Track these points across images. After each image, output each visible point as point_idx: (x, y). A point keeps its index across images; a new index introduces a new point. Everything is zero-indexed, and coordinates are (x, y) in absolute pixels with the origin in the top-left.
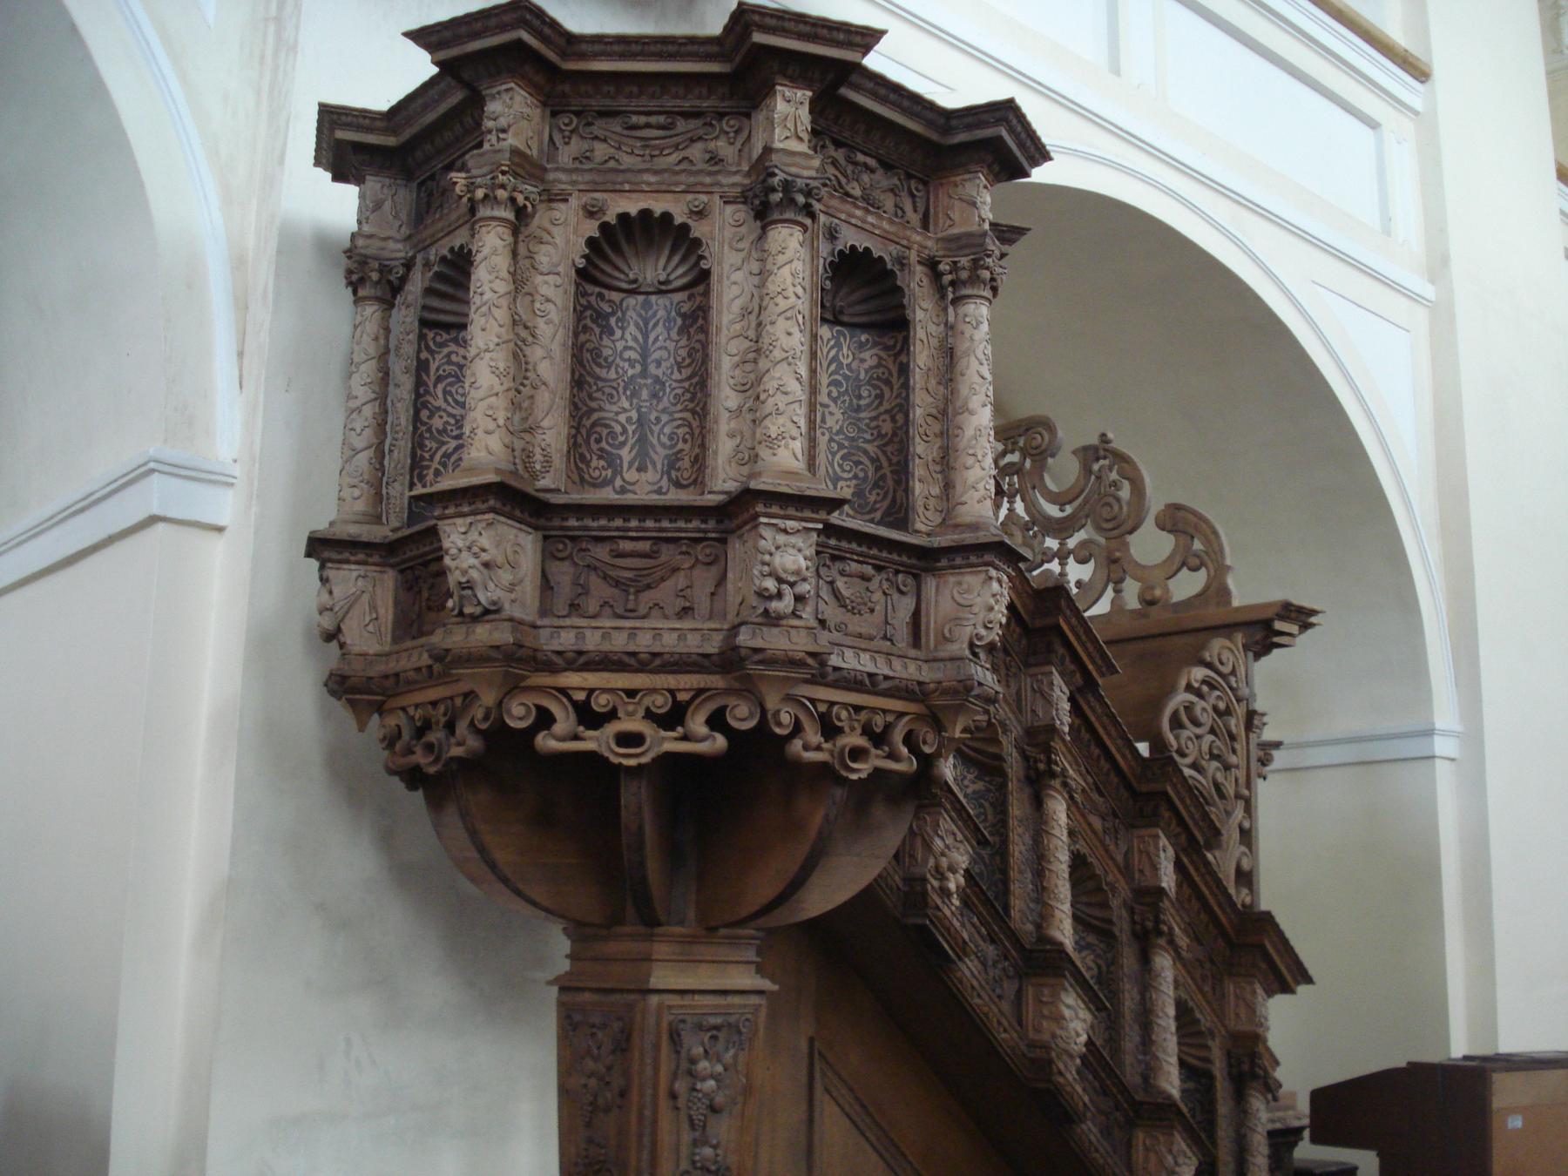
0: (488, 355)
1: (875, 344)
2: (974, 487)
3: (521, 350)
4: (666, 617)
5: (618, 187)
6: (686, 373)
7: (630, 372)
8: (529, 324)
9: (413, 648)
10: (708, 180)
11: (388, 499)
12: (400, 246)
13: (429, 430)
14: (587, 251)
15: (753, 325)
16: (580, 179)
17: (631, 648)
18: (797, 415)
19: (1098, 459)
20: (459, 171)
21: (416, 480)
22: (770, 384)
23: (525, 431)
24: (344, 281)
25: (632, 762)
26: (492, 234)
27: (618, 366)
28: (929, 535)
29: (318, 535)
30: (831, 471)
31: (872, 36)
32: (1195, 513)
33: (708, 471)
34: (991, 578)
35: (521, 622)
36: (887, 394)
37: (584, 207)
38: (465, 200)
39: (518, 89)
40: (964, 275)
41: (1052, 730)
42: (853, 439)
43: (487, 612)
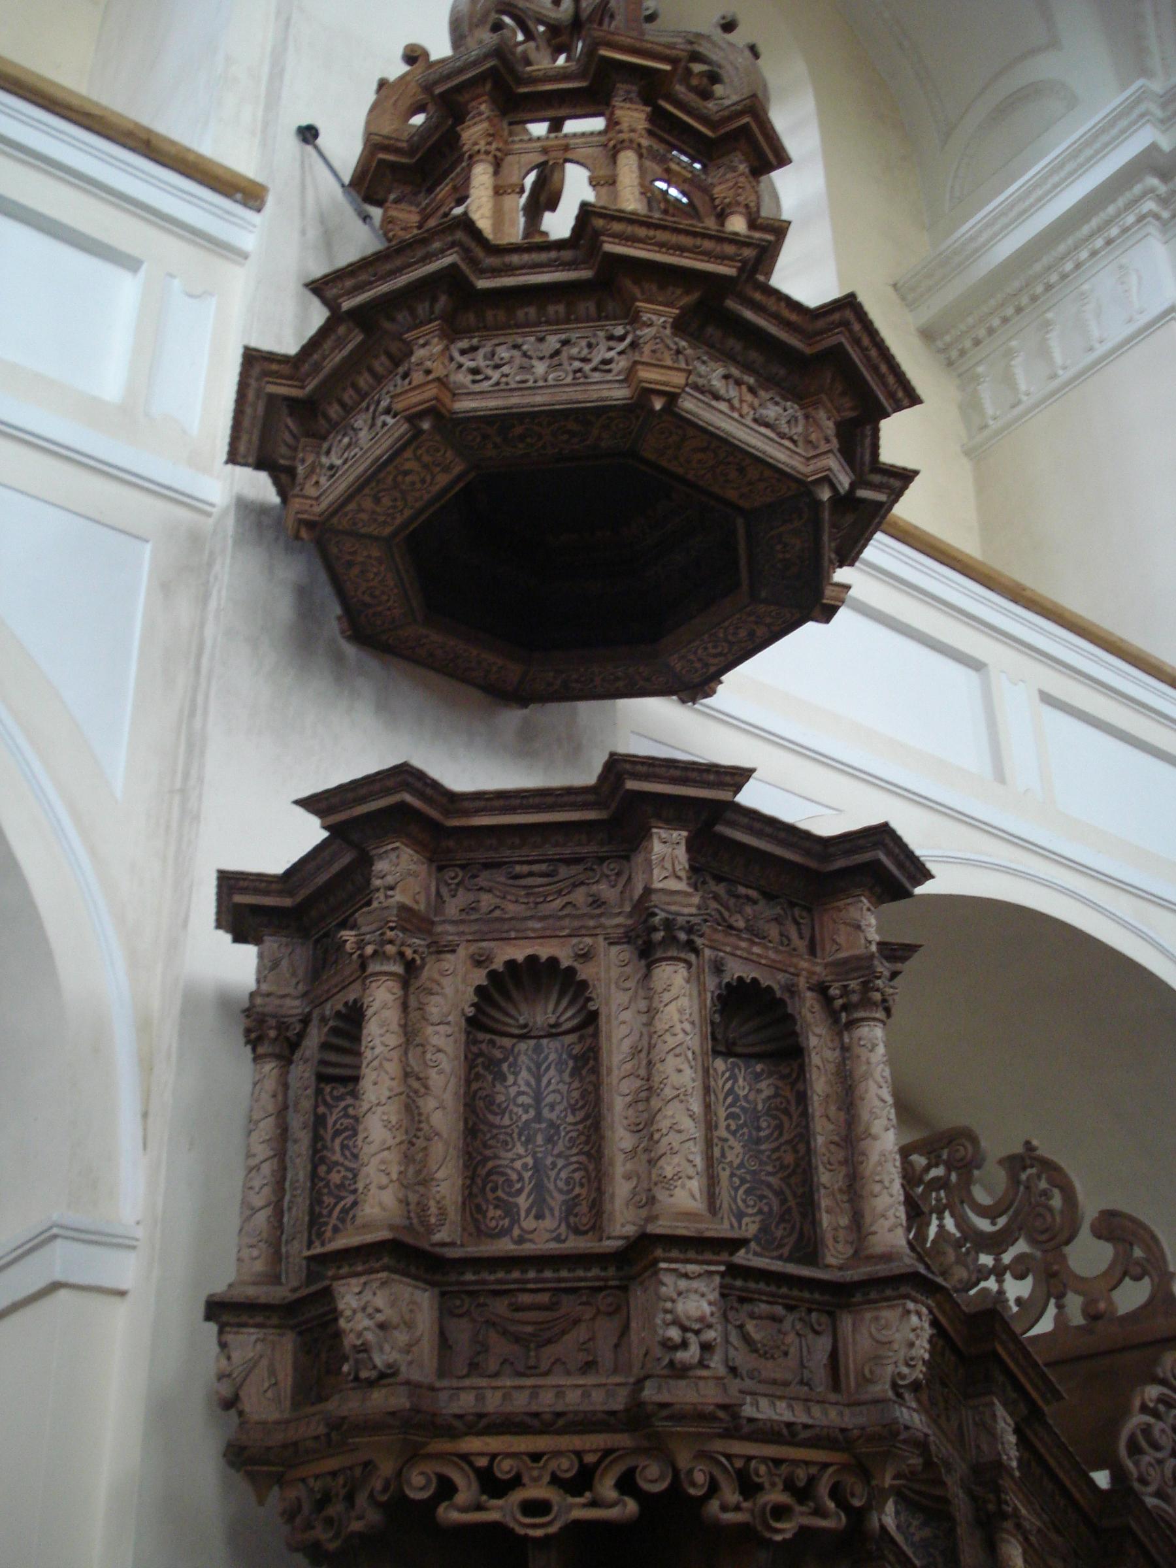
0: (380, 1109)
1: (770, 1075)
2: (883, 1216)
3: (414, 1101)
4: (568, 1373)
5: (505, 935)
6: (580, 1115)
7: (525, 1117)
8: (421, 1075)
9: (314, 1415)
10: (591, 923)
11: (287, 1257)
12: (297, 1003)
13: (327, 1185)
14: (476, 1000)
15: (644, 1062)
16: (467, 930)
17: (534, 1408)
18: (692, 1153)
19: (1024, 1168)
20: (352, 929)
21: (314, 1237)
22: (664, 1124)
23: (419, 1183)
24: (242, 1040)
25: (539, 1533)
26: (382, 989)
27: (511, 1112)
28: (841, 1268)
29: (216, 1299)
30: (734, 1207)
31: (741, 775)
32: (1134, 1220)
33: (605, 1216)
34: (908, 1312)
35: (418, 1385)
36: (786, 1125)
37: (472, 957)
38: (355, 956)
39: (403, 847)
40: (855, 998)
41: (999, 1466)
42: (754, 1173)
43: (383, 1376)
